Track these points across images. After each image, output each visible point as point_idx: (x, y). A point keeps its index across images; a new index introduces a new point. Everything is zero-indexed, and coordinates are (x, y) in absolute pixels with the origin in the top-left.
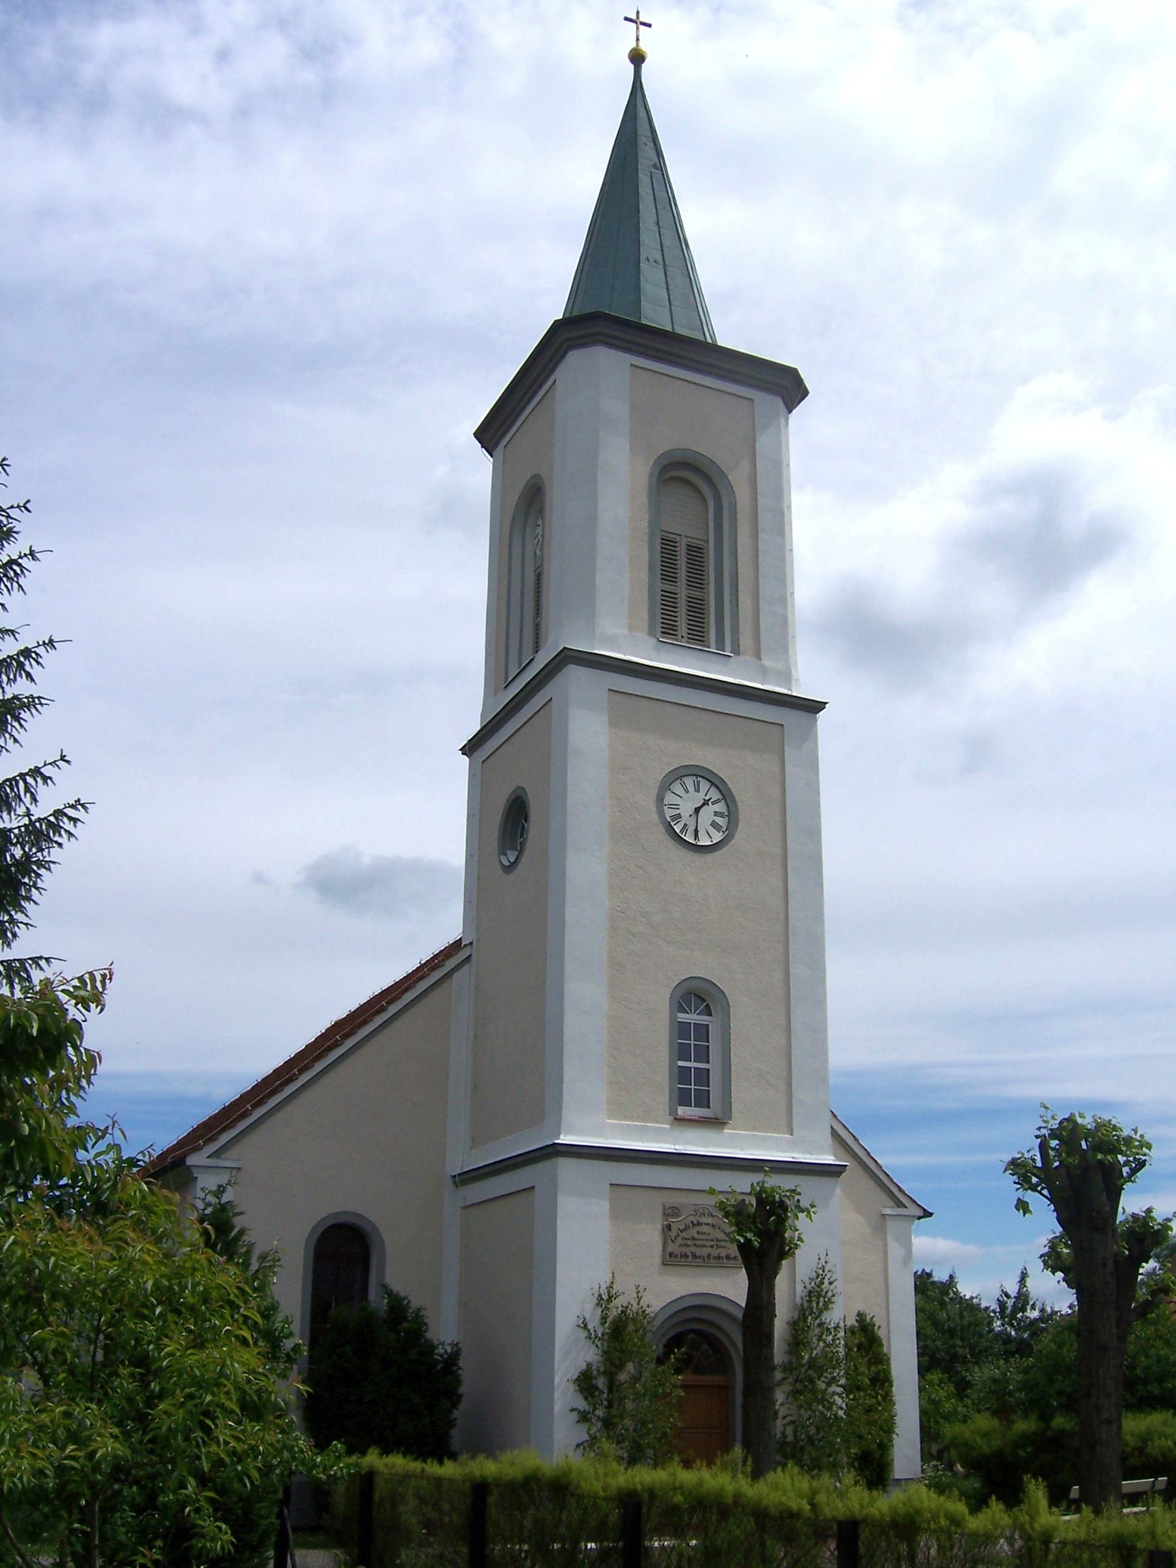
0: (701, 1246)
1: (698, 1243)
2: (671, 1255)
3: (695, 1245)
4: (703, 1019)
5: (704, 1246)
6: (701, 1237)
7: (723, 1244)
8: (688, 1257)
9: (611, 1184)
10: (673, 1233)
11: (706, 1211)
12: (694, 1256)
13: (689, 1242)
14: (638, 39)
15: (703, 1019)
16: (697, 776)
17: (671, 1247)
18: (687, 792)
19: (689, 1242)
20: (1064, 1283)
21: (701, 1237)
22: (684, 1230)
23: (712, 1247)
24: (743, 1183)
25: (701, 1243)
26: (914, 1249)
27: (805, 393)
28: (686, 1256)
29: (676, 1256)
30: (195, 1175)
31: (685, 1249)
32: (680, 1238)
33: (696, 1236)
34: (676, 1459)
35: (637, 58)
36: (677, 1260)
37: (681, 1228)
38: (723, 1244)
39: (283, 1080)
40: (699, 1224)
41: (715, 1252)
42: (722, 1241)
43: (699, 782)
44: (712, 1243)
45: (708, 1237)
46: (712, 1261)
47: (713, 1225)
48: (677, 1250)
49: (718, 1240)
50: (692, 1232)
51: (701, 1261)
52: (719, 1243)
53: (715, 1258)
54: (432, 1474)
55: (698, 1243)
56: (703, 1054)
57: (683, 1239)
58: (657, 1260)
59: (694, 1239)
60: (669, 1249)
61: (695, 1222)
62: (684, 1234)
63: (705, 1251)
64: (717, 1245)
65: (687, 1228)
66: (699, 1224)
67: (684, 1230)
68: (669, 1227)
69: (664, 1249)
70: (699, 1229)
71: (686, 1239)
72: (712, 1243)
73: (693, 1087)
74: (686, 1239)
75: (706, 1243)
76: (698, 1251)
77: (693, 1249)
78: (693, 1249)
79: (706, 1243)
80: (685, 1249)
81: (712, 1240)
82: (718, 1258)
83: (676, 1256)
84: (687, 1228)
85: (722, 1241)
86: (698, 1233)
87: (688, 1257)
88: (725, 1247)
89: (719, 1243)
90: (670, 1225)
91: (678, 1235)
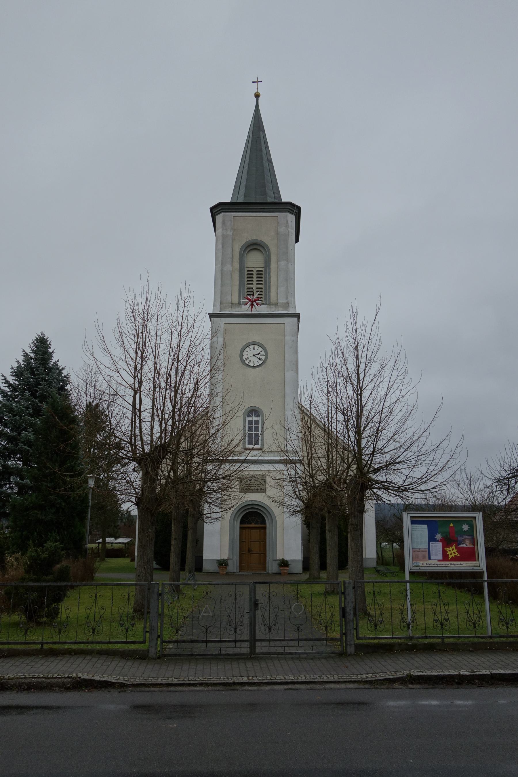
4: (256, 418)
12: (249, 490)
14: (257, 89)
15: (256, 418)
16: (254, 345)
18: (251, 350)
20: (339, 579)
24: (260, 473)
27: (212, 209)
35: (257, 96)
39: (90, 501)
41: (256, 488)
43: (255, 347)
50: (249, 482)
54: (46, 692)
56: (257, 429)
62: (246, 483)
63: (253, 488)
70: (251, 481)
73: (253, 439)
82: (257, 490)
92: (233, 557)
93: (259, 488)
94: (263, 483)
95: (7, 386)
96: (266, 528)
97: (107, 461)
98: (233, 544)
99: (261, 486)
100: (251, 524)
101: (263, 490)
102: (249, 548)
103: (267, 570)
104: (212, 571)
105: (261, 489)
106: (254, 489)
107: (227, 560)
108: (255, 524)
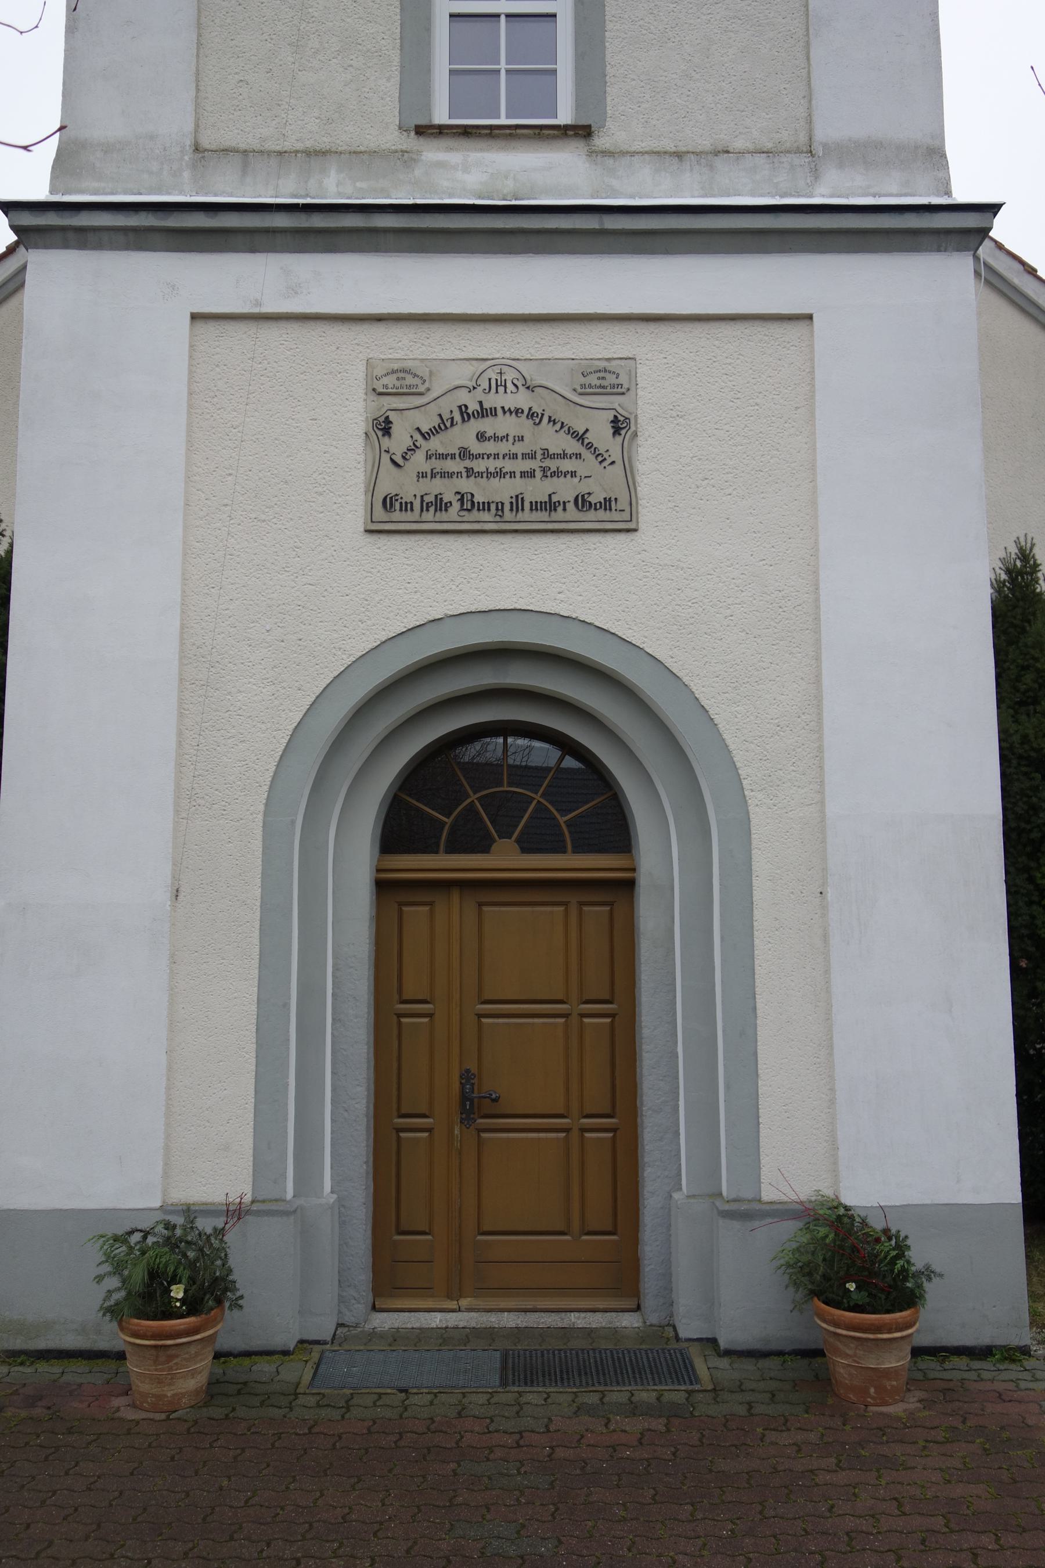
0: (490, 475)
1: (480, 466)
2: (388, 503)
3: (470, 472)
5: (500, 474)
6: (490, 447)
7: (566, 465)
8: (448, 505)
9: (195, 317)
10: (401, 438)
11: (510, 376)
13: (451, 466)
17: (390, 482)
19: (451, 466)
21: (490, 447)
22: (435, 431)
23: (530, 474)
25: (492, 465)
26: (569, 122)
28: (440, 505)
29: (407, 507)
30: (862, 1293)
31: (437, 486)
32: (419, 457)
33: (476, 448)
34: (722, 1348)
36: (408, 516)
37: (425, 429)
38: (566, 465)
40: (484, 412)
41: (537, 490)
42: (564, 456)
44: (527, 465)
45: (519, 449)
46: (526, 515)
47: (531, 415)
48: (407, 486)
49: (546, 454)
50: (464, 435)
51: (485, 516)
52: (553, 464)
53: (535, 507)
55: (480, 466)
57: (428, 457)
58: (355, 515)
59: (465, 453)
60: (386, 487)
61: (473, 407)
62: (435, 444)
63: (503, 490)
64: (544, 470)
65: (443, 425)
66: (484, 412)
67: (435, 431)
68: (385, 427)
69: (372, 489)
70: (487, 425)
71: (443, 457)
72: (527, 465)
74: (443, 457)
75: (508, 466)
76: (482, 491)
77: (465, 485)
78: (465, 485)
79: (508, 466)
80: (437, 486)
81: (532, 456)
82: (550, 505)
83: (407, 507)
84: (443, 425)
85: (564, 456)
86: (481, 437)
87: (448, 505)
88: (573, 474)
89: (553, 464)
90: (387, 421)
91: (414, 448)
92: (306, 1178)
93: (565, 490)
94: (601, 433)
95: (109, 1274)
96: (629, 886)
97: (134, 1293)
98: (473, 861)
99: (588, 464)
100: (483, 845)
101: (607, 504)
102: (466, 1076)
103: (649, 1302)
104: (71, 1341)
105: (582, 502)
106: (517, 505)
107: (236, 1212)
108: (527, 846)
